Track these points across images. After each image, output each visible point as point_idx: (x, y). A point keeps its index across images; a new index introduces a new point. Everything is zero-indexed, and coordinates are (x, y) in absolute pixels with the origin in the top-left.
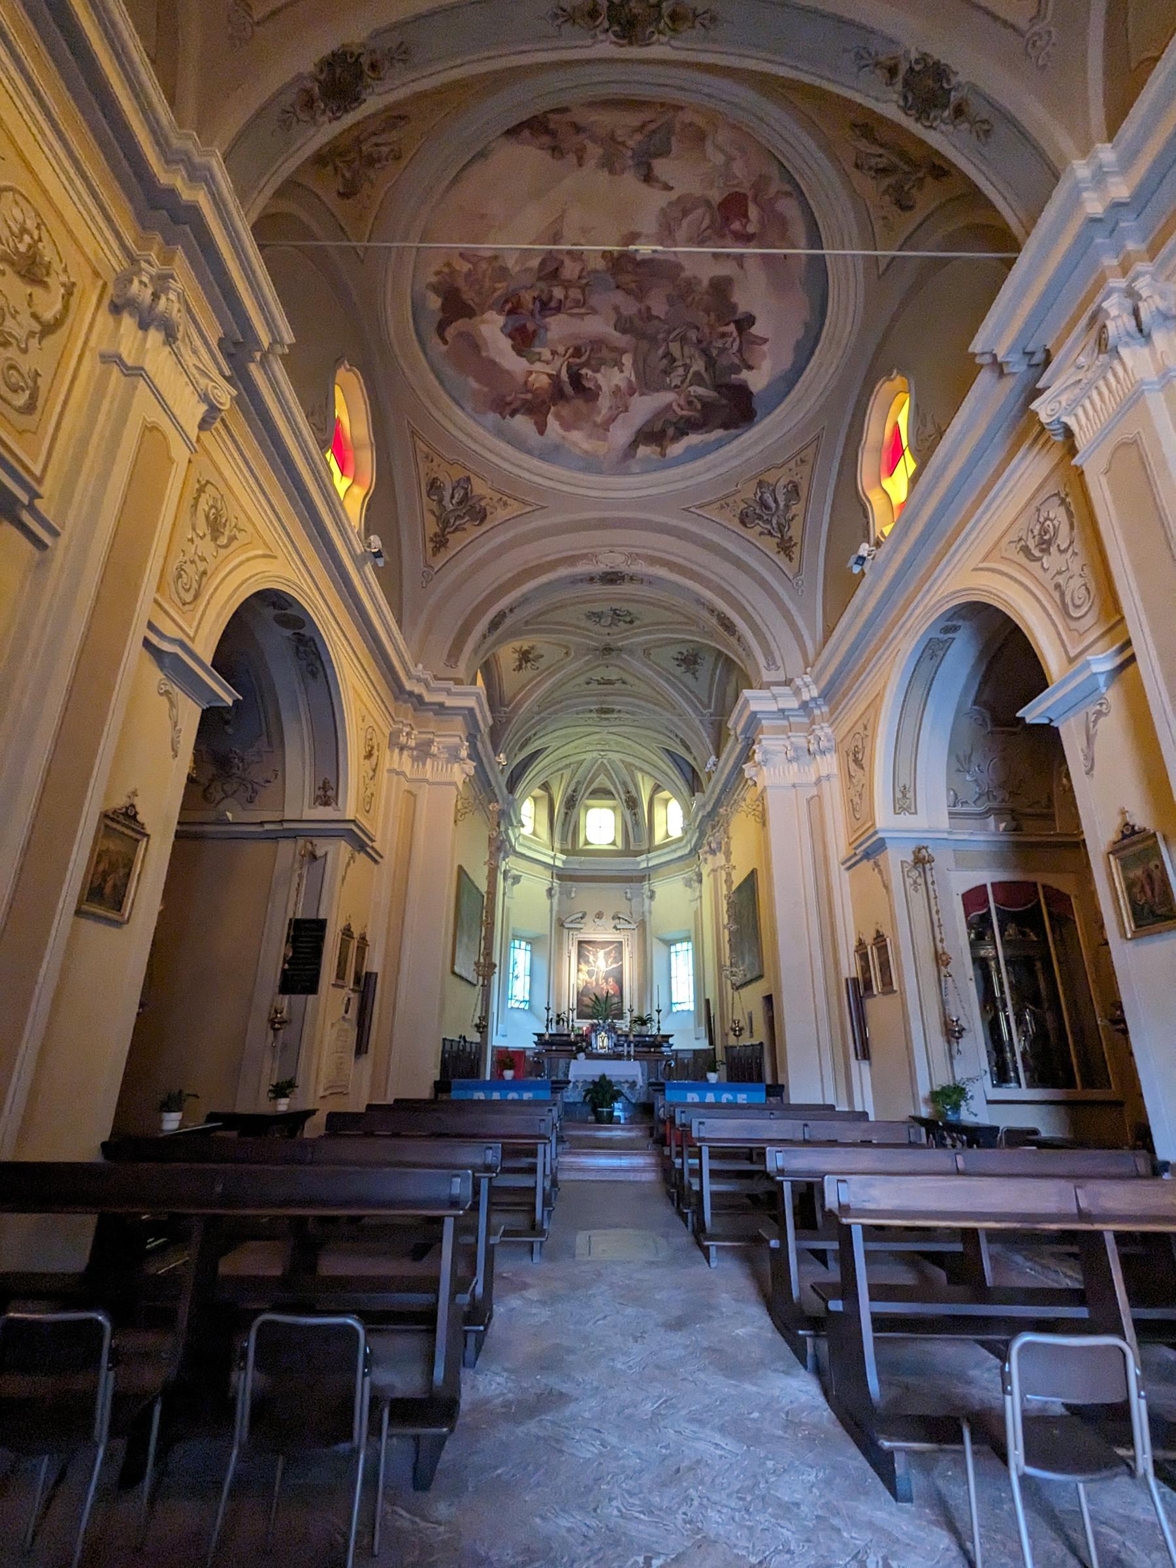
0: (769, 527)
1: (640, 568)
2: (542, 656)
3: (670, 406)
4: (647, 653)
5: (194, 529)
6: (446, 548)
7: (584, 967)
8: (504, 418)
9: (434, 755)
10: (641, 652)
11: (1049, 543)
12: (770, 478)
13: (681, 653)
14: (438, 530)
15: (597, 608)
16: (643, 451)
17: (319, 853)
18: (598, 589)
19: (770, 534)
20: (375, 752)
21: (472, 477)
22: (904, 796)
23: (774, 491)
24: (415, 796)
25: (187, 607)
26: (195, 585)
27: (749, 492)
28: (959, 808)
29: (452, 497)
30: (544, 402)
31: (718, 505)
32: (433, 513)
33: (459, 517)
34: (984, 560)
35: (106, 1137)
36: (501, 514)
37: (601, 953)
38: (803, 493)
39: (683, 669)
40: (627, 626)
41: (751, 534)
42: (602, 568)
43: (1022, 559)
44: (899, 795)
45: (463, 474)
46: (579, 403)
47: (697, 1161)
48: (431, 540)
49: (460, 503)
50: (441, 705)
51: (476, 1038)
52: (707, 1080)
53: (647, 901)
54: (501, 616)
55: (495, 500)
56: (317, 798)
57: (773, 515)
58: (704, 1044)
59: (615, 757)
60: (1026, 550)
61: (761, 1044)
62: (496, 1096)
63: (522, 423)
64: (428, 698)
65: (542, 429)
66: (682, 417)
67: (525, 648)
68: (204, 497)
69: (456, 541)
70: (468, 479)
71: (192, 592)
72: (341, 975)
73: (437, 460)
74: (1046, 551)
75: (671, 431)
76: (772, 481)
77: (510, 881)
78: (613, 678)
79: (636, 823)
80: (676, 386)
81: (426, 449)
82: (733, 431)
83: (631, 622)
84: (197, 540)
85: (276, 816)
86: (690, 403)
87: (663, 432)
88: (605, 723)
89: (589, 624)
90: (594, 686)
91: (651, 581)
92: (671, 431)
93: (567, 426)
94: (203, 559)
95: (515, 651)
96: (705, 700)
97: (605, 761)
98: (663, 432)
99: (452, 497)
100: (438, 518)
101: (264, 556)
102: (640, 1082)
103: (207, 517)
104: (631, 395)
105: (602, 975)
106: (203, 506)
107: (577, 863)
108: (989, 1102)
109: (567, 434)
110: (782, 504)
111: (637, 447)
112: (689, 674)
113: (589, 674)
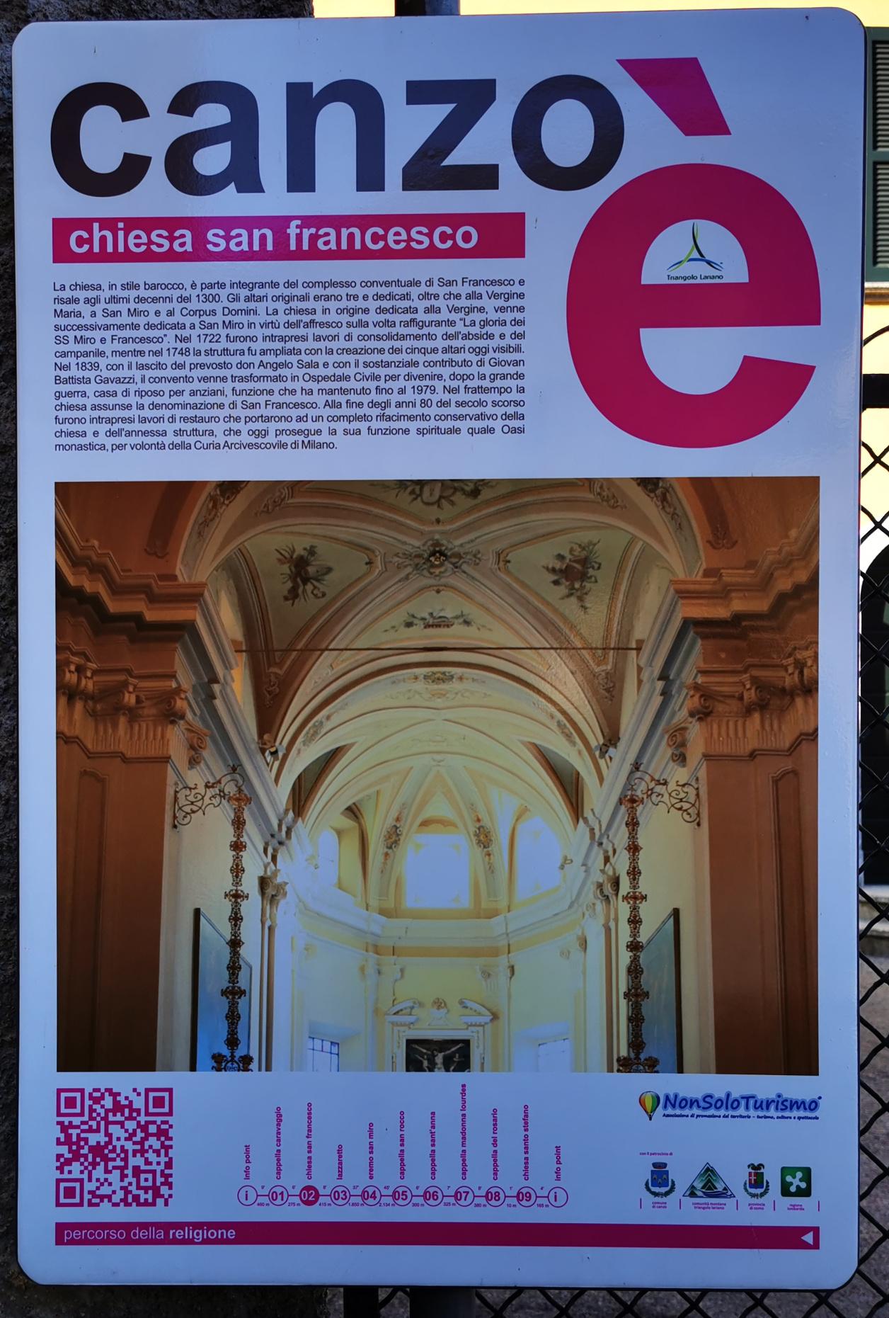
2: (329, 570)
4: (502, 558)
9: (130, 710)
10: (490, 560)
13: (561, 557)
24: (102, 781)
39: (562, 590)
40: (471, 502)
47: (867, 285)
50: (137, 618)
61: (175, 578)
64: (113, 606)
67: (299, 551)
78: (449, 614)
79: (491, 869)
88: (439, 702)
112: (573, 599)
113: (410, 607)
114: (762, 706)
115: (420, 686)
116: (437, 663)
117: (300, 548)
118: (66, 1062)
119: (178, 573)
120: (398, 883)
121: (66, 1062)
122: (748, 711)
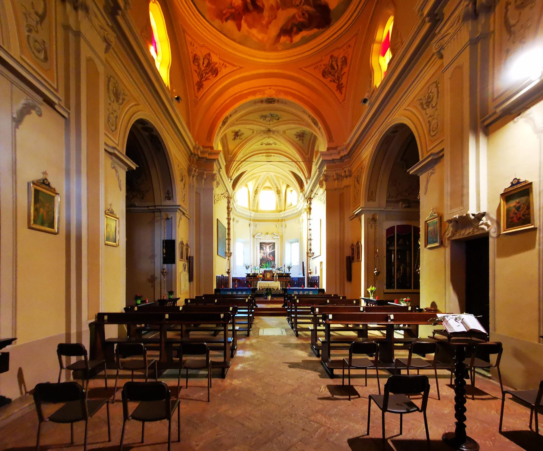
0: (333, 78)
1: (282, 97)
3: (294, 17)
5: (110, 99)
6: (203, 88)
7: (262, 251)
8: (223, 22)
11: (429, 102)
12: (335, 54)
14: (199, 80)
15: (264, 113)
16: (283, 39)
17: (170, 217)
18: (265, 105)
19: (334, 81)
20: (184, 179)
21: (211, 53)
22: (372, 195)
23: (337, 60)
25: (114, 132)
26: (114, 123)
27: (327, 60)
28: (390, 199)
29: (203, 63)
30: (239, 13)
31: (313, 67)
32: (196, 71)
33: (207, 73)
34: (408, 106)
35: (125, 306)
36: (224, 72)
37: (268, 247)
38: (349, 61)
40: (277, 121)
41: (326, 81)
42: (265, 97)
43: (420, 107)
44: (370, 195)
45: (207, 52)
46: (255, 14)
48: (196, 85)
49: (206, 66)
51: (227, 275)
52: (488, 360)
53: (284, 229)
54: (227, 118)
55: (221, 64)
56: (166, 197)
57: (335, 72)
58: (302, 276)
59: (273, 174)
60: (422, 104)
62: (235, 293)
63: (230, 25)
65: (239, 27)
66: (300, 21)
68: (111, 84)
69: (207, 85)
70: (209, 54)
71: (114, 126)
72: (182, 257)
73: (196, 45)
74: (428, 106)
75: (295, 29)
76: (336, 56)
77: (235, 222)
78: (271, 142)
79: (280, 200)
80: (298, 6)
81: (190, 39)
82: (321, 30)
83: (278, 119)
84: (112, 104)
85: (152, 204)
86: (303, 14)
87: (292, 29)
89: (262, 120)
90: (264, 145)
91: (285, 103)
92: (295, 29)
93: (250, 26)
94: (115, 111)
95: (232, 132)
96: (306, 152)
97: (269, 176)
98: (292, 29)
99: (203, 63)
100: (198, 74)
101: (135, 105)
102: (280, 288)
103: (113, 92)
104: (278, 9)
105: (268, 254)
106: (111, 88)
107: (259, 216)
108: (384, 293)
109: (250, 30)
110: (340, 67)
111: (280, 37)
114: (338, 179)
115: (264, 157)
116: (268, 153)
117: (237, 130)
118: (394, 288)
119: (214, 146)
120: (258, 204)
121: (394, 288)
122: (335, 180)
